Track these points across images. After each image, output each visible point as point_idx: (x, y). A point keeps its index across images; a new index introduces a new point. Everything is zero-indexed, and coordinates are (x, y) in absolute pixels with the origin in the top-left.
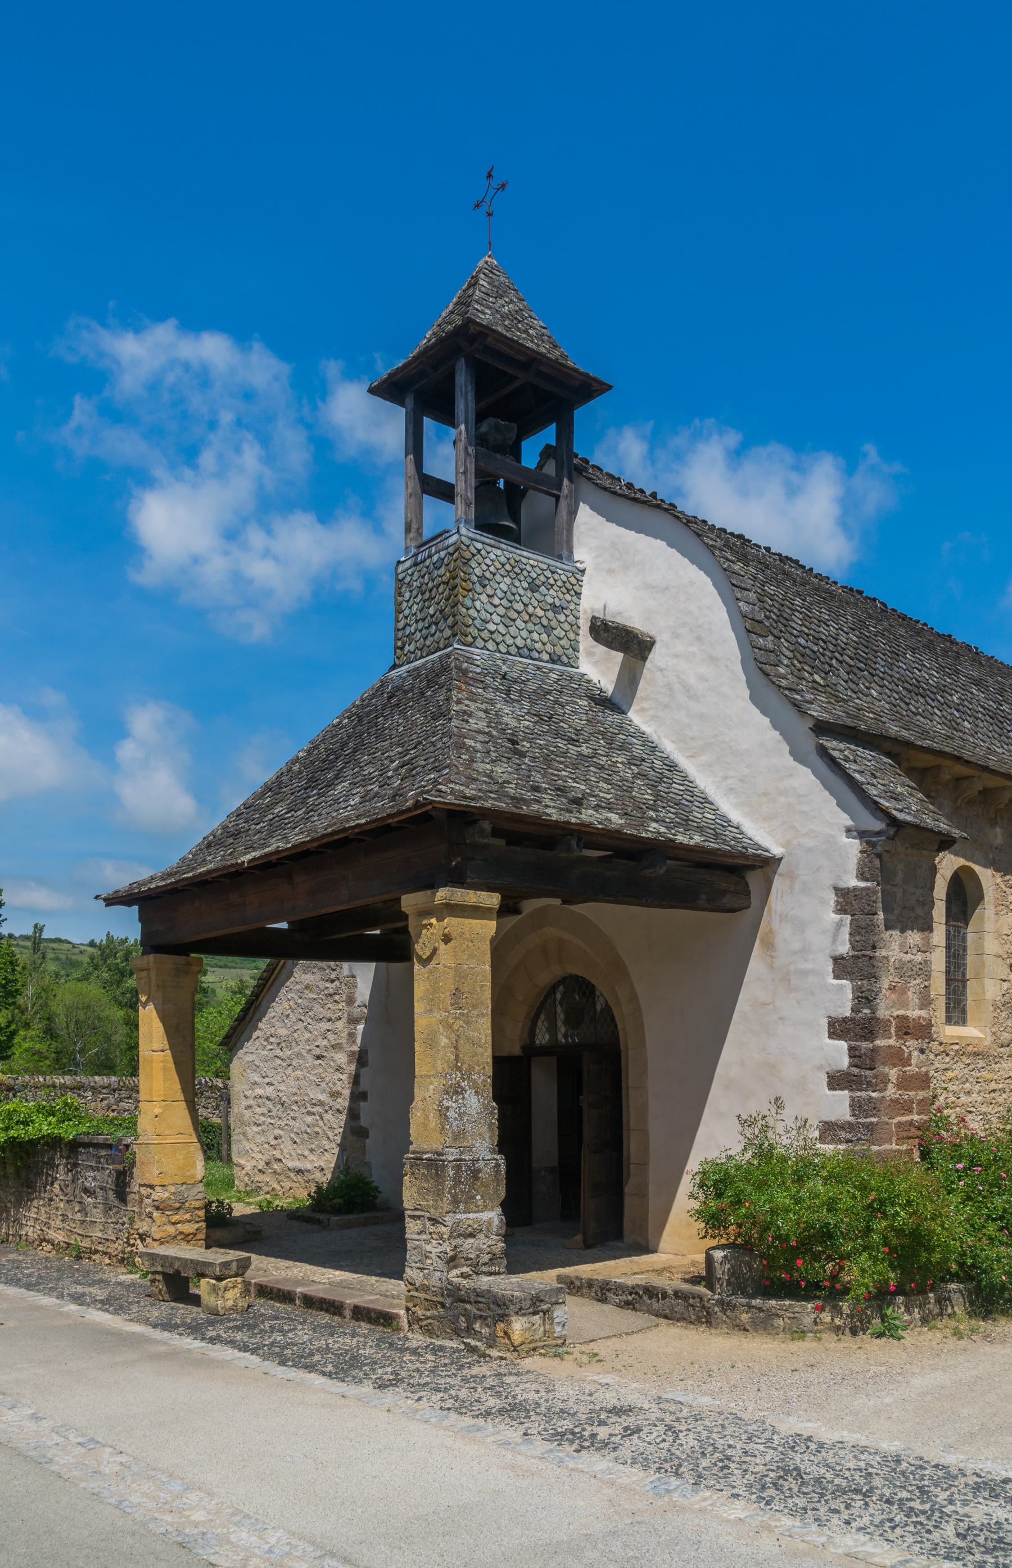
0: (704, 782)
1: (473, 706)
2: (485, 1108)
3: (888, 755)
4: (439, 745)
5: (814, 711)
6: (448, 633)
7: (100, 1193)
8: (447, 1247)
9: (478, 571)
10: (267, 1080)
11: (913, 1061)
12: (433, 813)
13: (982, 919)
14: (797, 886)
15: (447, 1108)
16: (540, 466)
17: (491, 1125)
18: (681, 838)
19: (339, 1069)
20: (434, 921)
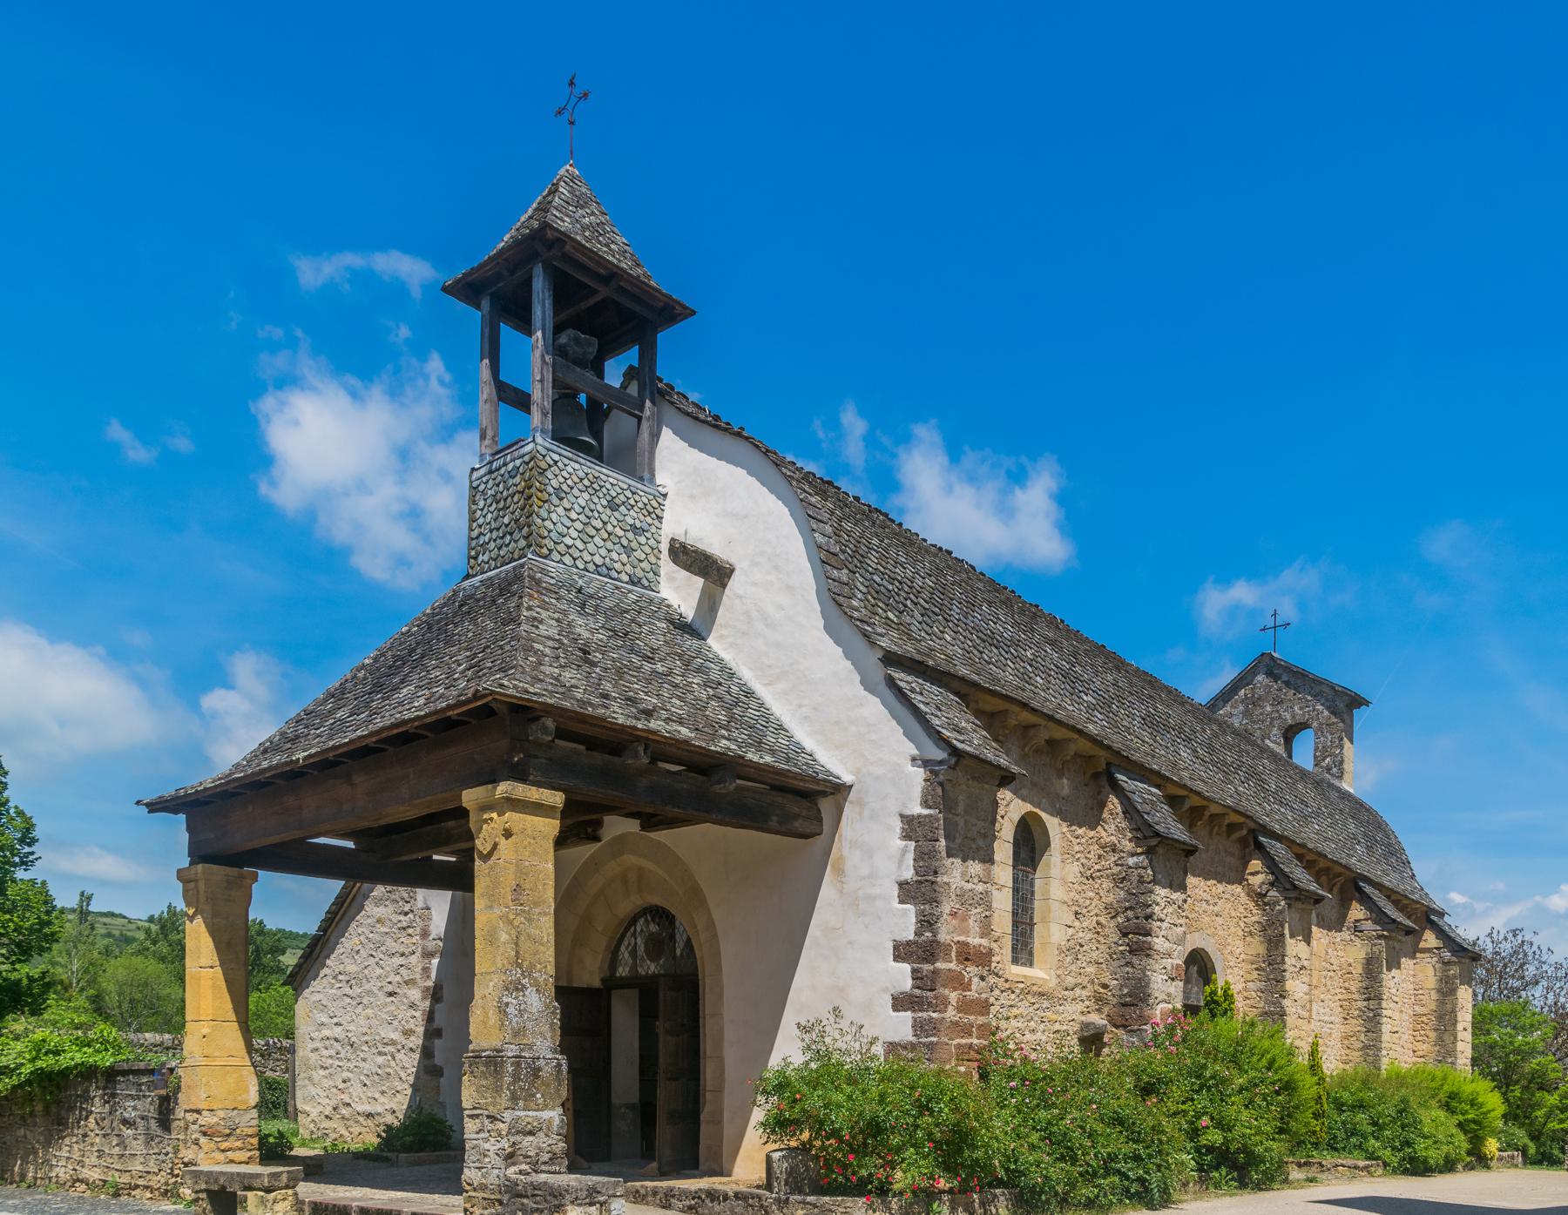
0: (781, 710)
1: (544, 614)
2: (547, 1007)
3: (956, 694)
4: (507, 648)
6: (523, 543)
7: (141, 1123)
8: (505, 1144)
9: (554, 483)
11: (974, 987)
12: (493, 705)
13: (1048, 865)
14: (866, 813)
16: (624, 386)
17: (552, 1024)
18: (752, 756)
19: (412, 1006)
20: (494, 815)
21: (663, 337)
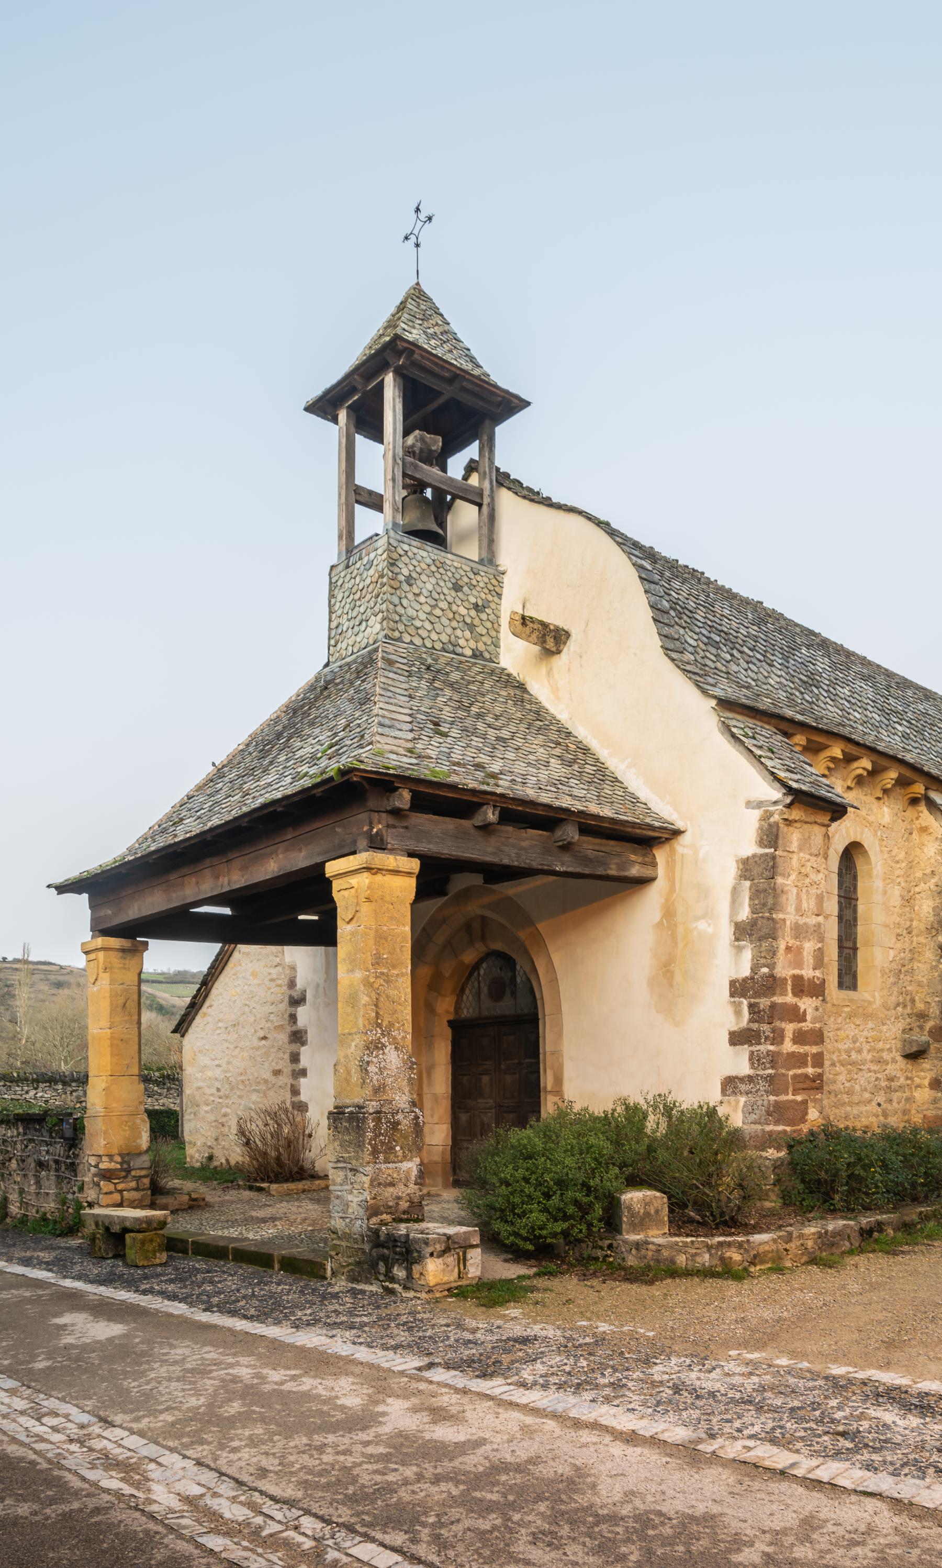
2: (405, 1063)
5: (717, 692)
10: (217, 1062)
11: (808, 1018)
15: (368, 1063)
17: (410, 1079)
21: (501, 430)
